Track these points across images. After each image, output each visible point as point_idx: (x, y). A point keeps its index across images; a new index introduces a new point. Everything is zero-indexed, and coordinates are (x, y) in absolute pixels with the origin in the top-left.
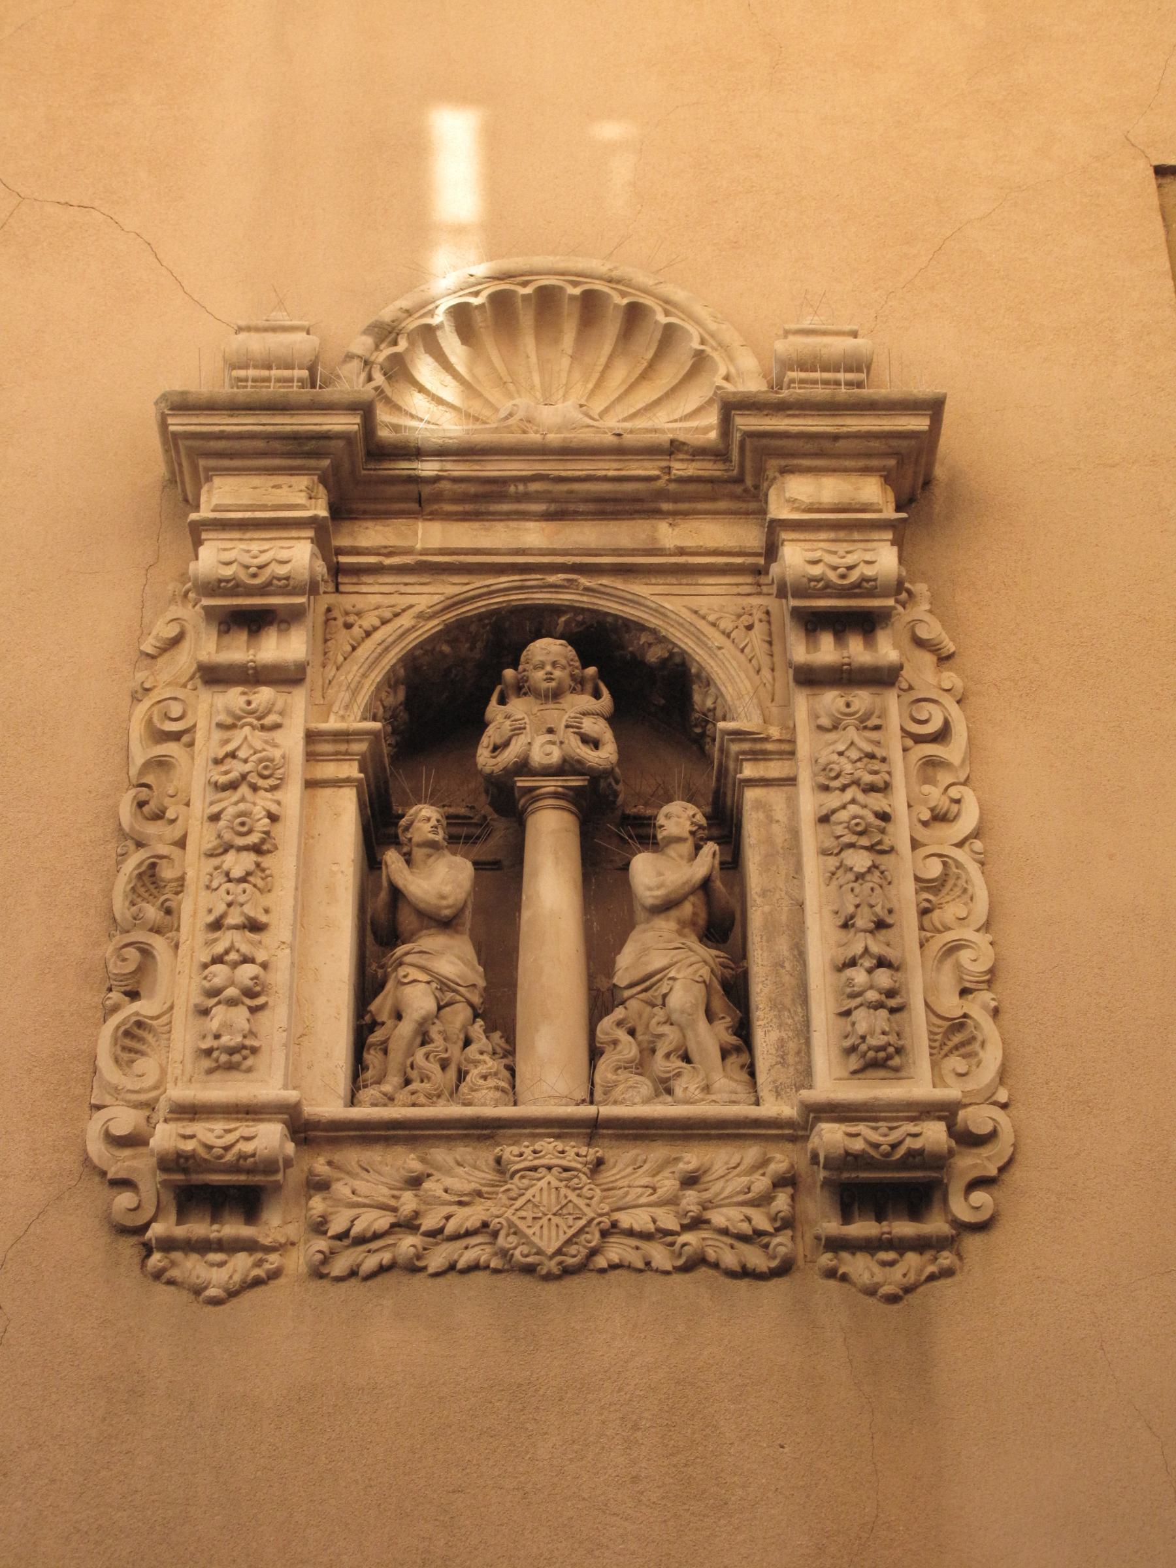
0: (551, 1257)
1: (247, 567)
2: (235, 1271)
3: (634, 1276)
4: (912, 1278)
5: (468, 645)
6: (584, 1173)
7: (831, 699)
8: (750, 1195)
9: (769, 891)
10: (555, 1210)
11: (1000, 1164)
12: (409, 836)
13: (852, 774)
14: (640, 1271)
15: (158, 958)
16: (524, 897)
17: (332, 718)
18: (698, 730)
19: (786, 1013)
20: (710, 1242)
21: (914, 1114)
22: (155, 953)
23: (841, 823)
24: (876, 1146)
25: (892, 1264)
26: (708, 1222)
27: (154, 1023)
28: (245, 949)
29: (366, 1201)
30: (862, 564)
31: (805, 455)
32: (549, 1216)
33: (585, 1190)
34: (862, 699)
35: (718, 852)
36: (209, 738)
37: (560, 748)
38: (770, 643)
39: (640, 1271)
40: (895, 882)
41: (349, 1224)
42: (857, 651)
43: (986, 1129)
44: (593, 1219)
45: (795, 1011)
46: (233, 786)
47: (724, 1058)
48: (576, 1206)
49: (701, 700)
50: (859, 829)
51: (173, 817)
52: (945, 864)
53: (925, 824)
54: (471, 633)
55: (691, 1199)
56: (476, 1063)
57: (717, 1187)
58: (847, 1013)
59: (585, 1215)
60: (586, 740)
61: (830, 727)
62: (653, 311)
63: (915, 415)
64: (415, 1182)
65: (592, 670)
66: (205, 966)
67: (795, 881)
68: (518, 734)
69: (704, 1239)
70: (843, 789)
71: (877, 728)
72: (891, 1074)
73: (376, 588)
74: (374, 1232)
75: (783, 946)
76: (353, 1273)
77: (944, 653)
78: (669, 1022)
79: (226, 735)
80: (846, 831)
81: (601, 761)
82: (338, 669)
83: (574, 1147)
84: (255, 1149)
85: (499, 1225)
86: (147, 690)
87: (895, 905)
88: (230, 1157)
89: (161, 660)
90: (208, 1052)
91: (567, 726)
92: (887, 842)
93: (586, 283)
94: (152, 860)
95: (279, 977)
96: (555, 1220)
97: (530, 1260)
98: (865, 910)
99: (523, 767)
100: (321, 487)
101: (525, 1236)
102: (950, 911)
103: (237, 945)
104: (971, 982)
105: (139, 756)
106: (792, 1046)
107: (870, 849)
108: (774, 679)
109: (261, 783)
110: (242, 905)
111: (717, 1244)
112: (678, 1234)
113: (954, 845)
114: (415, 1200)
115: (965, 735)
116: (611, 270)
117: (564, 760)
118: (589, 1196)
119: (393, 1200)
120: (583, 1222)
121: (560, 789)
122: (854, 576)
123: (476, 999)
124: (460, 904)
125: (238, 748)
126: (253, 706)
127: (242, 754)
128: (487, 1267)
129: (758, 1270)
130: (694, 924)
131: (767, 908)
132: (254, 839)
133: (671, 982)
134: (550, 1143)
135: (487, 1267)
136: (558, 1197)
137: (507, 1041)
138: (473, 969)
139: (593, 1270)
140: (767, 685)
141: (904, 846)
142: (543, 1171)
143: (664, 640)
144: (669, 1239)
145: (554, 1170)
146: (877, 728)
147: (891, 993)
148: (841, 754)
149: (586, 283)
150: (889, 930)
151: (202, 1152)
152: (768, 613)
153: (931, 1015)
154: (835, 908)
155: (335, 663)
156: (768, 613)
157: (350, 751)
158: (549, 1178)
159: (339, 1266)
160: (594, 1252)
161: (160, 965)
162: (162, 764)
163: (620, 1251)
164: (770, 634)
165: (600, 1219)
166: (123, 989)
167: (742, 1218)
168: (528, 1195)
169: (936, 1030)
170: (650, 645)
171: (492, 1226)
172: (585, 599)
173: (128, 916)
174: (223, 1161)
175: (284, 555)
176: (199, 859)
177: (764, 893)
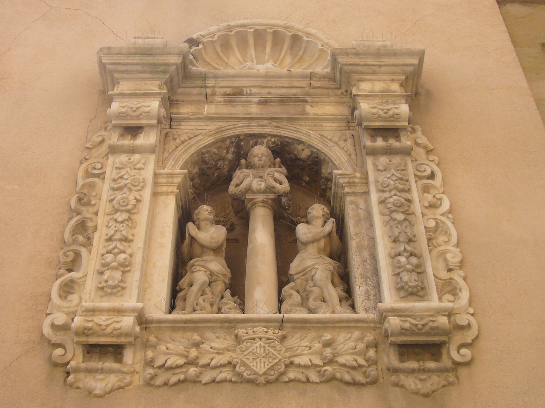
0: (261, 376)
1: (132, 108)
2: (108, 383)
3: (301, 385)
4: (435, 387)
5: (225, 151)
6: (277, 341)
7: (383, 160)
8: (356, 350)
9: (359, 233)
10: (263, 355)
11: (473, 338)
12: (198, 217)
13: (394, 185)
14: (304, 382)
15: (83, 256)
16: (249, 241)
17: (166, 169)
18: (324, 187)
19: (369, 280)
20: (337, 371)
21: (431, 313)
22: (82, 254)
23: (390, 203)
24: (416, 325)
25: (424, 380)
26: (337, 362)
27: (79, 280)
28: (121, 247)
29: (173, 352)
30: (394, 108)
31: (368, 73)
32: (260, 358)
33: (278, 347)
34: (397, 160)
35: (335, 222)
36: (112, 173)
37: (265, 182)
38: (355, 146)
39: (304, 382)
40: (416, 226)
41: (165, 362)
42: (393, 142)
43: (465, 323)
44: (281, 359)
45: (373, 279)
46: (120, 189)
47: (340, 301)
48: (273, 354)
49: (325, 171)
50: (398, 205)
51: (94, 204)
52: (437, 223)
53: (426, 207)
54: (227, 145)
55: (328, 352)
56: (226, 304)
57: (340, 347)
58: (398, 274)
59: (278, 357)
60: (276, 180)
61: (383, 170)
62: (303, 37)
63: (412, 58)
64: (197, 345)
65: (278, 160)
66: (103, 255)
67: (370, 230)
68: (246, 177)
69: (334, 369)
70: (391, 191)
71: (404, 170)
72: (420, 299)
73: (187, 127)
74: (176, 365)
75: (366, 254)
76: (166, 384)
77: (429, 149)
78: (315, 286)
79: (119, 171)
80: (392, 206)
81: (283, 189)
82: (169, 154)
83: (272, 330)
84: (121, 326)
85: (236, 362)
86: (86, 159)
87: (416, 233)
88: (109, 330)
89: (93, 150)
90: (102, 289)
91: (268, 174)
92: (411, 211)
93: (275, 28)
94: (83, 219)
95: (138, 260)
96: (263, 360)
97: (251, 377)
98: (403, 234)
99: (249, 189)
100: (165, 86)
101: (250, 367)
102: (442, 239)
103: (118, 246)
104: (453, 266)
105: (81, 182)
106: (372, 292)
107: (403, 213)
108: (357, 158)
109: (133, 188)
110: (121, 231)
111: (341, 371)
112: (323, 367)
113: (440, 215)
114: (197, 352)
115: (441, 176)
116: (285, 24)
117: (267, 188)
118: (279, 350)
119: (185, 352)
120: (276, 361)
121: (265, 199)
122: (390, 113)
123: (227, 281)
124: (219, 243)
125: (124, 175)
126: (132, 160)
127: (126, 177)
128: (231, 381)
129: (361, 382)
130: (324, 250)
131: (358, 240)
132: (129, 207)
133: (316, 270)
134: (260, 328)
135: (231, 381)
136: (265, 350)
137: (241, 300)
138: (225, 269)
139: (281, 382)
140: (354, 160)
141: (419, 214)
142: (258, 340)
143: (310, 146)
144: (318, 369)
145: (263, 340)
146: (404, 170)
147: (418, 266)
148: (388, 178)
149: (275, 28)
150: (414, 243)
151: (96, 328)
152: (353, 135)
153: (436, 279)
154: (390, 235)
155: (168, 151)
156: (353, 135)
157: (173, 182)
158: (260, 342)
159: (159, 381)
160: (282, 374)
161: (83, 258)
162: (92, 186)
163: (294, 374)
164: (354, 143)
165: (285, 360)
166: (66, 268)
167: (353, 359)
168: (251, 349)
169: (439, 284)
170: (303, 150)
171: (233, 363)
172: (275, 131)
173: (71, 240)
174: (105, 331)
175: (148, 104)
176: (104, 216)
177: (356, 234)
